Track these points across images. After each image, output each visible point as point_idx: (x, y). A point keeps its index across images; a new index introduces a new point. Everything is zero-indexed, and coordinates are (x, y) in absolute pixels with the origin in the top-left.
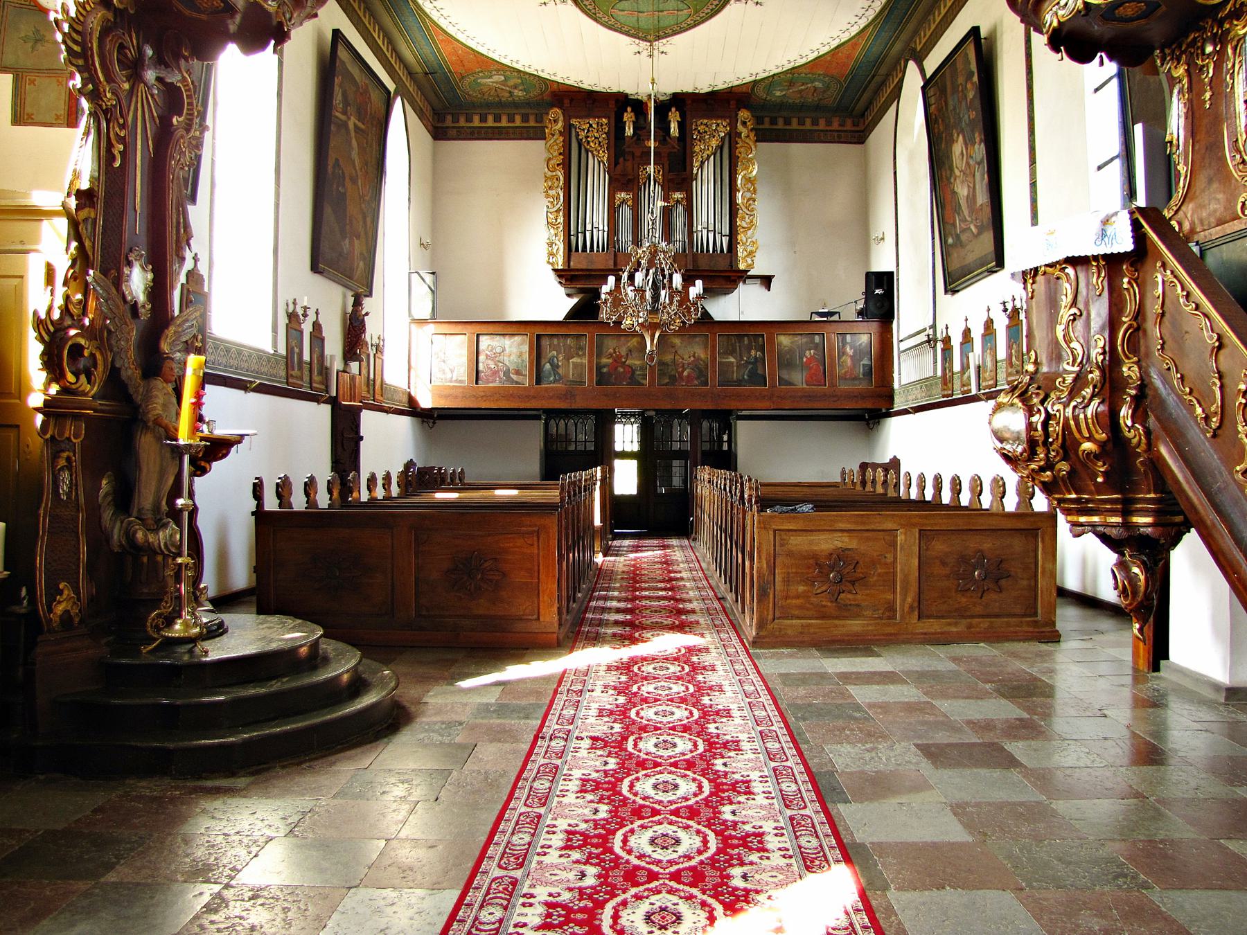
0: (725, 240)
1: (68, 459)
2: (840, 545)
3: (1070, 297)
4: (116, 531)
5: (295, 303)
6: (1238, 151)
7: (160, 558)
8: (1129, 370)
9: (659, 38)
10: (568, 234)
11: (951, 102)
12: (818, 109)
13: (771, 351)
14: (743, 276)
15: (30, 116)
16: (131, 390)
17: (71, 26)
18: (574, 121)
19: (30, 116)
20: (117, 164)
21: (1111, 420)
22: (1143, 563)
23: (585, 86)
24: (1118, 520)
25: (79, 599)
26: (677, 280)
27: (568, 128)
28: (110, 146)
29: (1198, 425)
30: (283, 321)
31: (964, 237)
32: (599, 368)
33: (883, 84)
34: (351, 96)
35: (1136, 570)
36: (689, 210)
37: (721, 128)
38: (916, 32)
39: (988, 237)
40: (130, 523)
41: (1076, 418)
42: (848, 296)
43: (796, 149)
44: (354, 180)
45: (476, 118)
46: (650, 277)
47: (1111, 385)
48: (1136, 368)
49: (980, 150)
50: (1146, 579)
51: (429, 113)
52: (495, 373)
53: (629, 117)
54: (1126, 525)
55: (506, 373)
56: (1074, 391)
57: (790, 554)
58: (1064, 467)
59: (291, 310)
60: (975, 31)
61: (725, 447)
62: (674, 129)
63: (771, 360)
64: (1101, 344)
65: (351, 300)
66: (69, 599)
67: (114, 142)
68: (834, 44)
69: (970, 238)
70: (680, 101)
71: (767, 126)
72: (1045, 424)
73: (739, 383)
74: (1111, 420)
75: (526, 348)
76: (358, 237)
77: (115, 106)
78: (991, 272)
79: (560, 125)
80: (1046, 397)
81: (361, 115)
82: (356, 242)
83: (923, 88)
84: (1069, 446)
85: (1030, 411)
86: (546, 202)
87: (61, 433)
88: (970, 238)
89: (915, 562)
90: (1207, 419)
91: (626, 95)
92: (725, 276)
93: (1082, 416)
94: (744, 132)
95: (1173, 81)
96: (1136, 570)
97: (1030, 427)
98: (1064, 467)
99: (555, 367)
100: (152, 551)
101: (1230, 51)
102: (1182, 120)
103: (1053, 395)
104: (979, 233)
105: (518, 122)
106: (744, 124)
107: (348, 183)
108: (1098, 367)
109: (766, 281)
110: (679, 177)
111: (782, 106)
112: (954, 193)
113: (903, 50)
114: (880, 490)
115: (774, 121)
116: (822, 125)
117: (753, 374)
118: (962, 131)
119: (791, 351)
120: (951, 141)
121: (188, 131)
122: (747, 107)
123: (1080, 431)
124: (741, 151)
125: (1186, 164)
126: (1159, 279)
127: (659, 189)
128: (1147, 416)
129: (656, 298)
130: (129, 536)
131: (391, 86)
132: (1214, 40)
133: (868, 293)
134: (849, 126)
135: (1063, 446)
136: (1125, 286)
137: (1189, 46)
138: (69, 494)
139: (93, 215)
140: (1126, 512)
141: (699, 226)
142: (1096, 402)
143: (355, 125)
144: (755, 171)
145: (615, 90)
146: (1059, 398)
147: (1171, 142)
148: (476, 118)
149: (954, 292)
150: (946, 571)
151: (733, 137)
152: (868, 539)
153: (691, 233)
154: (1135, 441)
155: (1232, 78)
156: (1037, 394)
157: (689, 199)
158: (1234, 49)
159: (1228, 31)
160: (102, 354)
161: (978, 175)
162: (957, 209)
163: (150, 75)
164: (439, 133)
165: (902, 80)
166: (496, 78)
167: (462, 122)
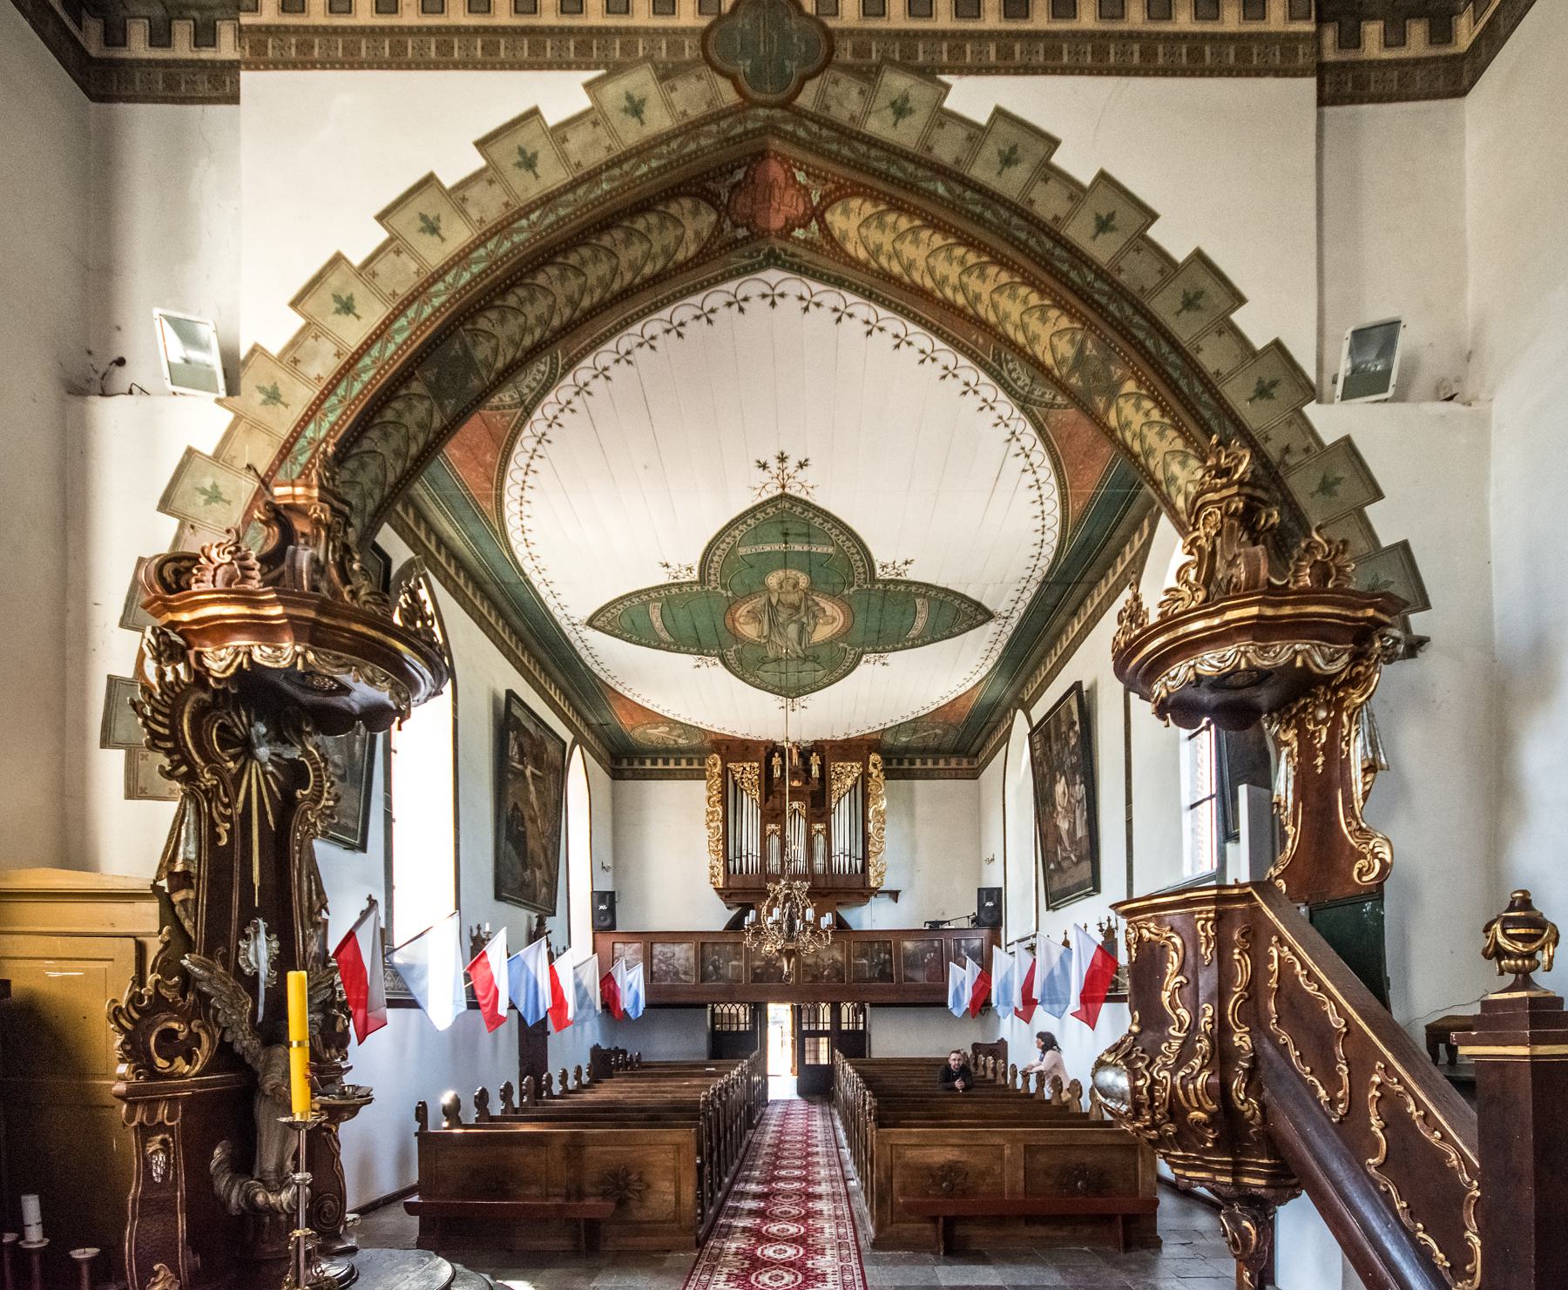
0: (859, 863)
1: (164, 1142)
2: (950, 1157)
3: (1176, 964)
4: (234, 1194)
5: (479, 928)
6: (1354, 817)
7: (283, 1218)
8: (1241, 1039)
9: (799, 695)
10: (726, 860)
11: (1055, 748)
12: (937, 752)
13: (898, 956)
14: (876, 892)
15: (143, 790)
16: (248, 1060)
17: (154, 710)
18: (730, 765)
19: (143, 790)
20: (224, 842)
21: (1223, 1092)
22: (1255, 1218)
23: (739, 735)
24: (1229, 1180)
25: (178, 1277)
26: (810, 914)
27: (725, 772)
28: (213, 825)
29: (1321, 1107)
30: (468, 944)
31: (1065, 864)
32: (753, 970)
33: (995, 728)
34: (527, 748)
35: (1246, 1224)
36: (828, 838)
37: (856, 768)
38: (1024, 685)
39: (1086, 866)
40: (250, 1186)
41: (1184, 1088)
42: (960, 910)
43: (919, 784)
44: (533, 820)
45: (648, 762)
46: (787, 911)
47: (1222, 1056)
48: (1247, 1039)
49: (1080, 790)
50: (1258, 1235)
51: (606, 756)
52: (667, 973)
53: (776, 761)
54: (1236, 1184)
55: (676, 973)
56: (1182, 1059)
57: (906, 1166)
58: (1171, 1129)
59: (475, 933)
60: (1077, 686)
61: (861, 1027)
62: (815, 771)
63: (898, 965)
64: (1210, 1012)
65: (535, 921)
66: (165, 1279)
67: (218, 821)
68: (952, 697)
69: (1069, 867)
70: (818, 747)
71: (894, 766)
72: (1151, 1090)
73: (871, 980)
74: (1223, 1092)
75: (692, 953)
76: (540, 868)
77: (217, 786)
78: (1088, 895)
79: (717, 770)
80: (1152, 1062)
81: (538, 762)
82: (538, 873)
83: (1030, 735)
84: (1176, 1111)
85: (1134, 1075)
86: (708, 832)
87: (151, 1118)
88: (1069, 867)
89: (1021, 1173)
90: (1333, 1103)
91: (774, 743)
92: (858, 889)
93: (1191, 1086)
94: (875, 772)
95: (1280, 744)
96: (1246, 1224)
97: (1135, 1090)
98: (1171, 1129)
99: (716, 968)
100: (272, 1211)
101: (1345, 718)
102: (1291, 782)
103: (1158, 1060)
104: (1077, 864)
105: (684, 765)
106: (875, 765)
107: (528, 824)
108: (1207, 1037)
109: (894, 895)
110: (819, 808)
111: (907, 749)
112: (1056, 827)
113: (1011, 701)
114: (990, 1075)
115: (900, 762)
116: (942, 764)
117: (882, 972)
118: (1064, 773)
119: (914, 954)
120: (1054, 782)
121: (317, 802)
122: (877, 751)
123: (1188, 1101)
124: (872, 787)
125: (1295, 825)
126: (1275, 954)
127: (803, 822)
128: (1262, 1090)
129: (791, 927)
130: (250, 1200)
131: (567, 736)
132: (1328, 705)
133: (981, 906)
134: (965, 764)
135: (1170, 1111)
136: (1236, 957)
137: (1299, 711)
138: (165, 1176)
139: (192, 895)
140: (1236, 1172)
141: (836, 850)
142: (1206, 1074)
143: (533, 774)
144: (883, 804)
145: (764, 738)
146: (1165, 1064)
147: (1278, 804)
148: (648, 762)
149: (1055, 909)
150: (1049, 1182)
151: (865, 776)
152: (977, 1153)
153: (830, 857)
154: (1249, 1114)
155: (1348, 744)
156: (1143, 1059)
157: (828, 829)
158: (1350, 717)
159: (1343, 700)
160: (207, 1032)
161: (1078, 813)
162: (1059, 840)
163: (263, 752)
164: (616, 774)
165: (1011, 726)
166: (662, 729)
167: (636, 765)
